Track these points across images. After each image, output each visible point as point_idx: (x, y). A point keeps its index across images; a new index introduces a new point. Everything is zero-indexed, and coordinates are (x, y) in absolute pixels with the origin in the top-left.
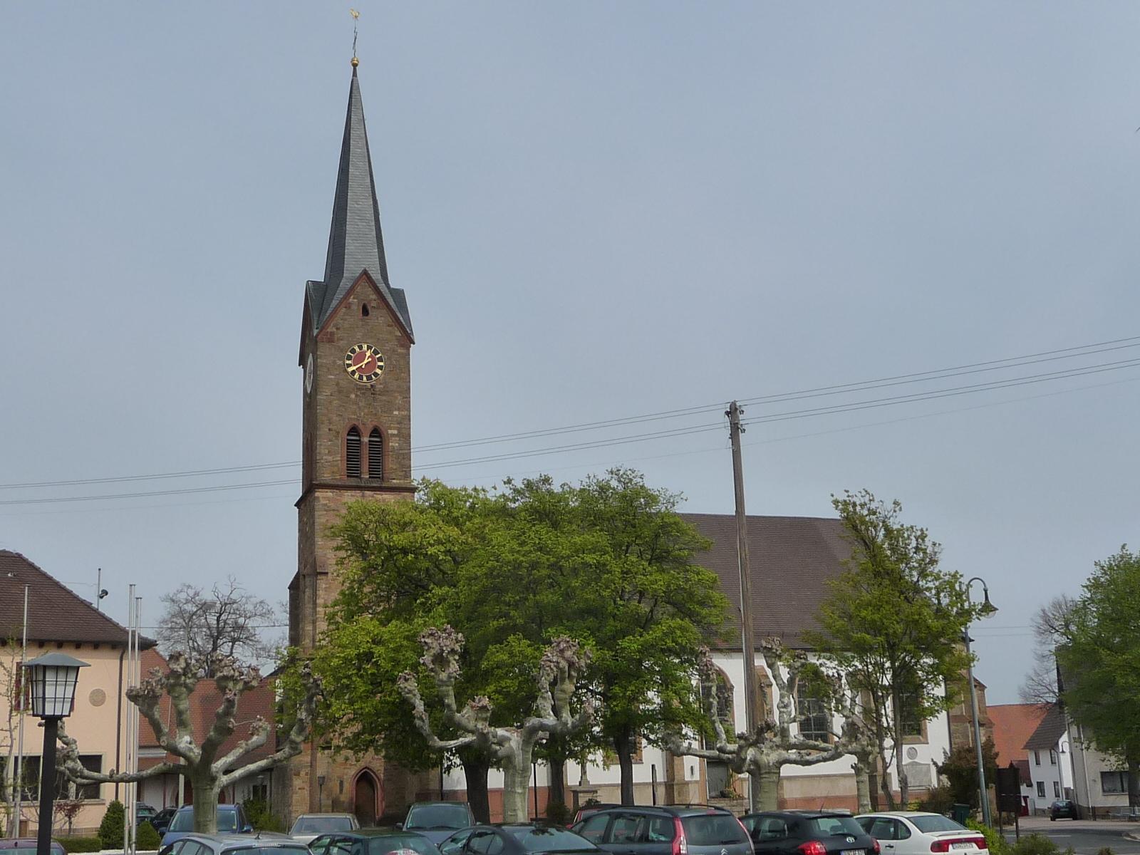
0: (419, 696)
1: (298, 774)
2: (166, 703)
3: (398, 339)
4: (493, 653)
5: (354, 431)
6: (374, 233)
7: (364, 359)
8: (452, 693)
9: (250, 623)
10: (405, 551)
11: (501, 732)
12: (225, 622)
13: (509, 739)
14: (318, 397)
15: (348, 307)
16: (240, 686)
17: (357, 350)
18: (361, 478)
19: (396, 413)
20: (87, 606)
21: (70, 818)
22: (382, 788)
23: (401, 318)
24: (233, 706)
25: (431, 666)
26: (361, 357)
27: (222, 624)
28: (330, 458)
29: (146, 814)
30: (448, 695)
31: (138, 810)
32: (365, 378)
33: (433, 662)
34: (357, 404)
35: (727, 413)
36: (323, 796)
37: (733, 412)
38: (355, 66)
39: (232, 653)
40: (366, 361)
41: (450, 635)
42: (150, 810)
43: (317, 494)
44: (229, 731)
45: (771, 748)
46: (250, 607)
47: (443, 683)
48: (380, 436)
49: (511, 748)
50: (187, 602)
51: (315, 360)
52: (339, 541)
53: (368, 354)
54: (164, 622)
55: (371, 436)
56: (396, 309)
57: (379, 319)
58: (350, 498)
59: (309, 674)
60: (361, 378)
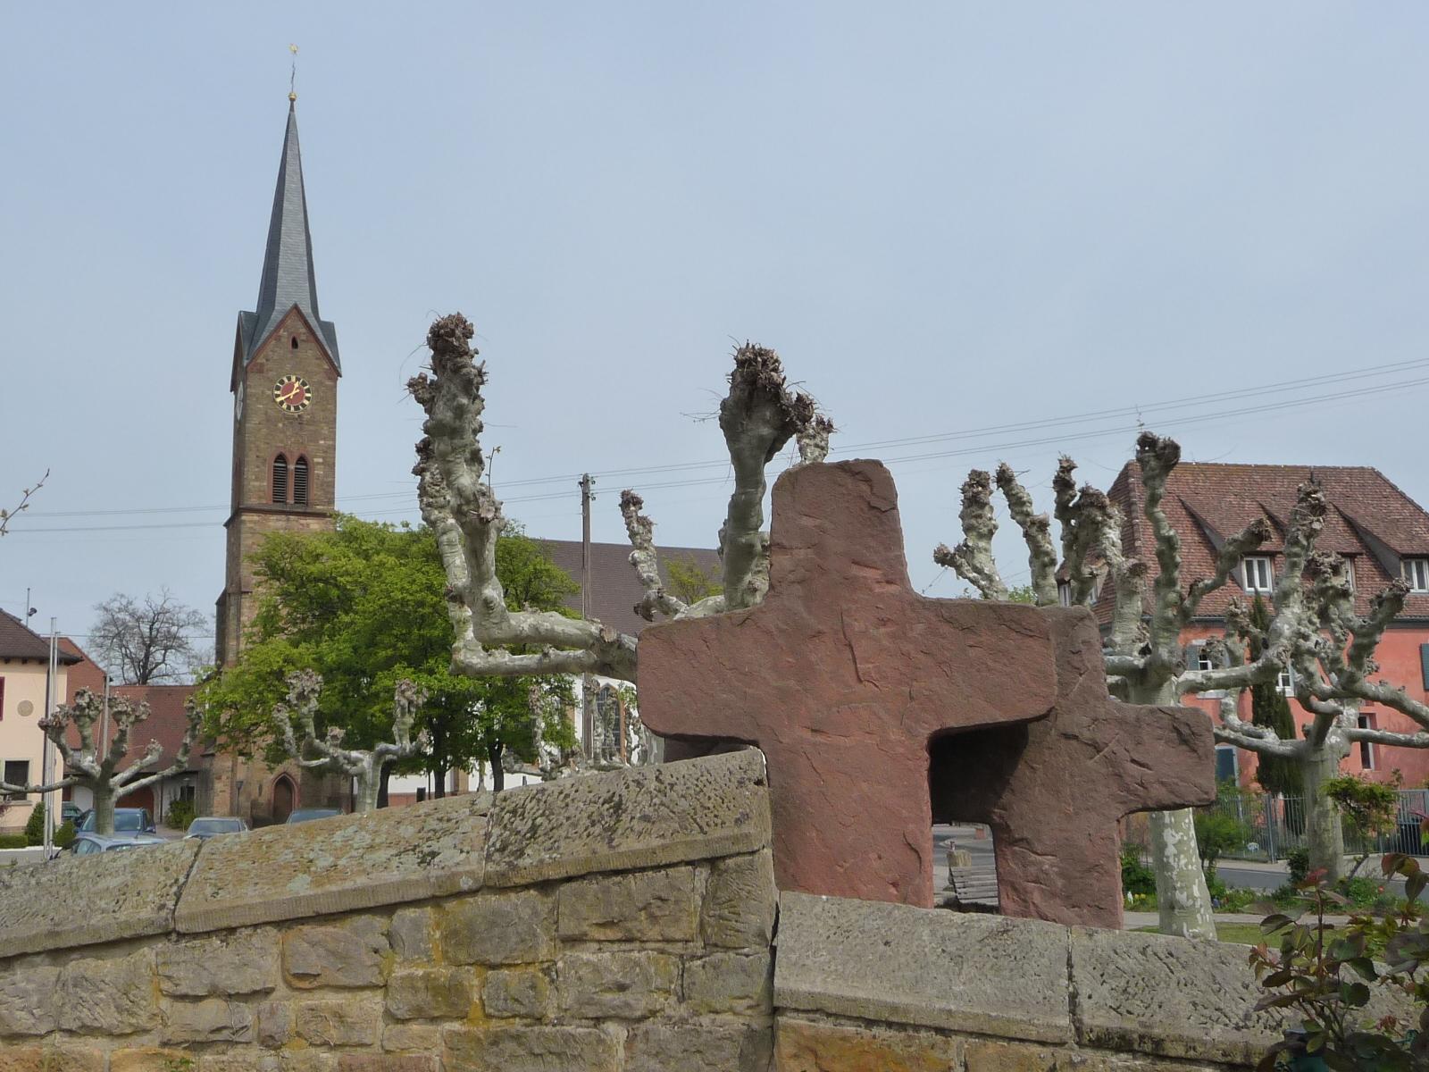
0: (289, 724)
1: (219, 778)
2: (71, 728)
3: (326, 372)
4: (381, 678)
5: (281, 458)
6: (306, 268)
7: (292, 390)
8: (312, 723)
9: (182, 633)
10: (317, 580)
11: (354, 754)
12: (158, 630)
13: (362, 760)
14: (247, 425)
15: (278, 339)
16: (132, 719)
17: (286, 381)
18: (286, 504)
19: (322, 442)
20: (16, 622)
21: (657, 1011)
22: (300, 790)
23: (330, 352)
24: (125, 735)
25: (295, 702)
26: (290, 388)
27: (154, 633)
28: (257, 484)
29: (72, 813)
30: (308, 726)
31: (63, 810)
32: (292, 409)
33: (297, 699)
34: (284, 432)
35: (580, 483)
36: (242, 798)
37: (585, 483)
38: (292, 100)
39: (164, 660)
40: (294, 392)
41: (311, 677)
42: (76, 810)
43: (244, 518)
44: (123, 754)
45: (586, 768)
46: (183, 616)
47: (305, 716)
48: (306, 464)
49: (363, 767)
50: (120, 610)
51: (245, 389)
52: (257, 567)
53: (296, 385)
54: (97, 629)
55: (297, 464)
56: (324, 343)
57: (308, 352)
58: (276, 523)
59: (193, 708)
60: (289, 408)
